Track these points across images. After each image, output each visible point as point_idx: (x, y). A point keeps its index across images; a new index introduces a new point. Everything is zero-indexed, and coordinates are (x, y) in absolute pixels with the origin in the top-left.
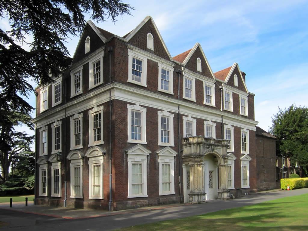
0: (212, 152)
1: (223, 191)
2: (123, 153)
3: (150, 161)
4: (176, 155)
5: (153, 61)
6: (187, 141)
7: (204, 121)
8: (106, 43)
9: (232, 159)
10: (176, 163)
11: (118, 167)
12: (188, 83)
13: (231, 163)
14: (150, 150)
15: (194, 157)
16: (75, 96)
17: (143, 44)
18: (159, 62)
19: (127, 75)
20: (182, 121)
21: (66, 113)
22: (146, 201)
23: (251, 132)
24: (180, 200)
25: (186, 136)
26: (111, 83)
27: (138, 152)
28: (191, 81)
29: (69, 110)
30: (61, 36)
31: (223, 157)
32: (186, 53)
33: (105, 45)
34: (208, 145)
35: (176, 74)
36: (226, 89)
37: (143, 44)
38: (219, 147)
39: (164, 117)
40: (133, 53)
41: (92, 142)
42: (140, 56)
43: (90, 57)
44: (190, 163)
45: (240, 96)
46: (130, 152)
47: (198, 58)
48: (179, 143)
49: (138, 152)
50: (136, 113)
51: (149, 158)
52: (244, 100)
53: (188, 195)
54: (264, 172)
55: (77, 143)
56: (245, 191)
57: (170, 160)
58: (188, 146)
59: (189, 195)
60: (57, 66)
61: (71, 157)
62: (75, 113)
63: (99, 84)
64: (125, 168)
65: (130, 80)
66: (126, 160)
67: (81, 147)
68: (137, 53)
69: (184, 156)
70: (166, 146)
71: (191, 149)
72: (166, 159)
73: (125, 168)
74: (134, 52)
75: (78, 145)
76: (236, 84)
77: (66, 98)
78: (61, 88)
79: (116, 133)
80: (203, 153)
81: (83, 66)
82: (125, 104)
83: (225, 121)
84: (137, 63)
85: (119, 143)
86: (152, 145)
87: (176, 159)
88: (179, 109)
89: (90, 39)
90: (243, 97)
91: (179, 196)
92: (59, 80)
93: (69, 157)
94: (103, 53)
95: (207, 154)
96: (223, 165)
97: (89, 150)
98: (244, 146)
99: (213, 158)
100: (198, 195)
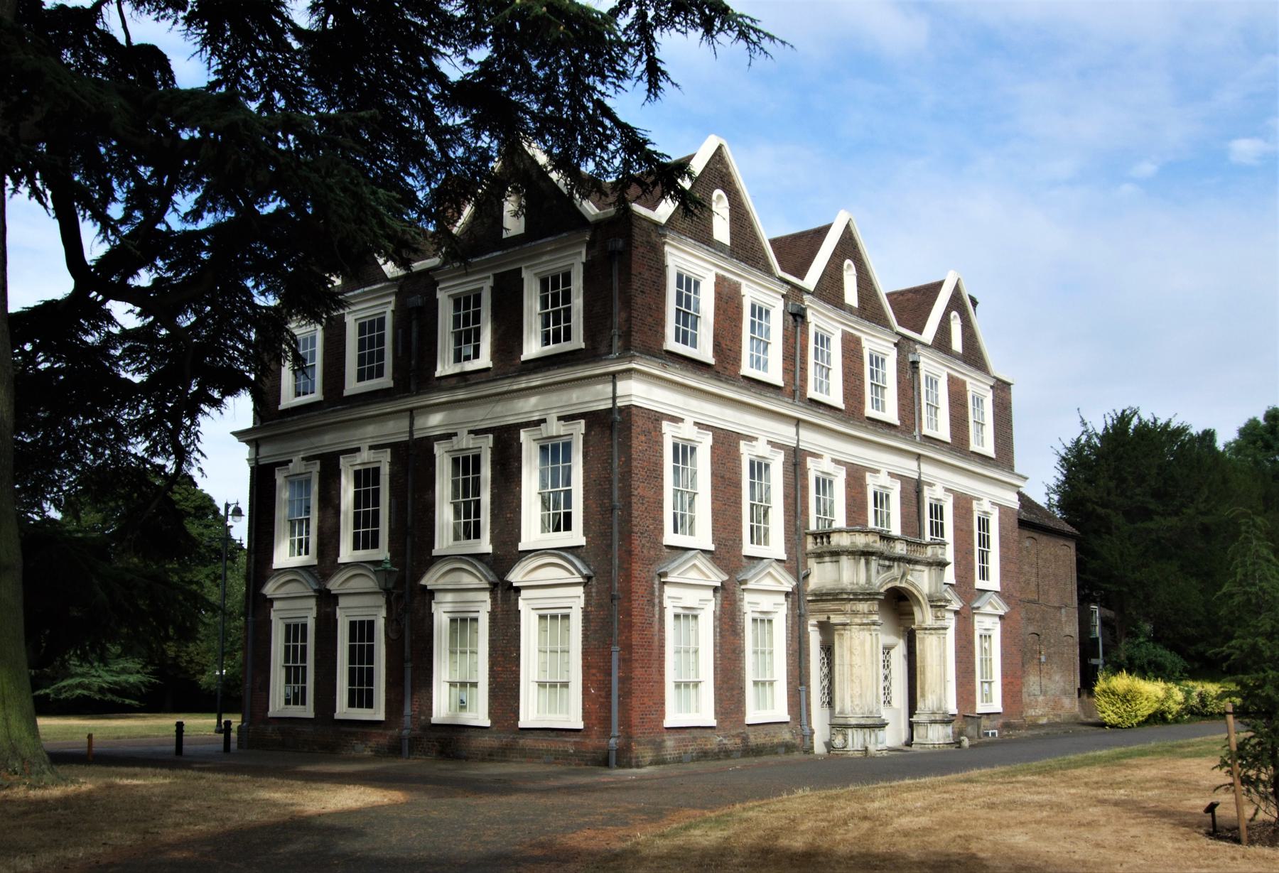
2: (653, 578)
12: (688, 289)
14: (728, 573)
18: (743, 282)
21: (412, 424)
23: (1004, 510)
27: (692, 576)
38: (918, 567)
39: (756, 460)
41: (532, 533)
45: (969, 387)
47: (848, 262)
63: (564, 347)
70: (762, 559)
71: (839, 571)
72: (766, 599)
73: (656, 627)
79: (635, 513)
81: (495, 275)
82: (656, 418)
84: (688, 284)
88: (797, 434)
90: (978, 388)
93: (430, 580)
99: (898, 604)
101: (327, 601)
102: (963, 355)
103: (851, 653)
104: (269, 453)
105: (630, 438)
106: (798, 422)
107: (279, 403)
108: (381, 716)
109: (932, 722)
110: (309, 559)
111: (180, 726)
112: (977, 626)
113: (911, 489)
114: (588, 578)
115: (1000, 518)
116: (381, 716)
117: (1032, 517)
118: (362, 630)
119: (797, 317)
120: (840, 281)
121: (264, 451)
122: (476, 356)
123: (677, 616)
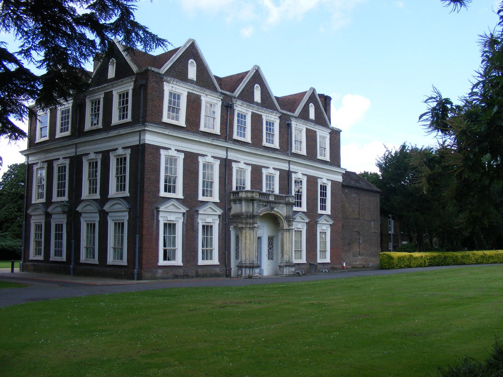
0: (271, 211)
1: (285, 264)
2: (154, 209)
3: (187, 220)
4: (221, 214)
5: (195, 94)
6: (237, 196)
7: (263, 169)
8: (138, 74)
9: (304, 221)
10: (221, 224)
11: (148, 226)
13: (300, 225)
14: (187, 206)
15: (245, 217)
16: (91, 129)
17: (183, 74)
19: (162, 113)
20: (231, 169)
21: (76, 150)
22: (181, 272)
23: (334, 183)
24: (226, 272)
25: (237, 189)
26: (142, 125)
27: (172, 209)
28: (245, 116)
29: (81, 147)
30: (81, 59)
31: (286, 219)
32: (241, 76)
33: (136, 76)
34: (266, 202)
35: (225, 108)
36: (297, 125)
37: (183, 74)
38: (280, 205)
40: (170, 86)
41: (113, 191)
42: (178, 89)
43: (115, 85)
44: (240, 226)
45: (318, 134)
46: (162, 208)
48: (227, 198)
49: (172, 209)
50: (171, 159)
51: (186, 216)
52: (324, 138)
53: (237, 266)
54: (359, 242)
55: (92, 191)
56: (322, 266)
57: (213, 220)
58: (237, 202)
59: (238, 267)
60: (69, 89)
61: (82, 209)
62: (91, 151)
64: (155, 227)
65: (165, 119)
66: (157, 218)
67: (97, 196)
68: (174, 86)
69: (233, 216)
72: (210, 217)
73: (155, 227)
74: (171, 85)
75: (93, 194)
76: (312, 116)
77: (78, 130)
78: (70, 114)
79: (146, 184)
80: (257, 213)
81: (105, 93)
82: (157, 149)
83: (293, 168)
84: (175, 97)
85: (149, 197)
86: (191, 203)
87: (221, 219)
88: (227, 153)
89: (116, 63)
90: (323, 134)
91: (224, 268)
92: (68, 105)
93: (79, 209)
94: (132, 84)
95: (263, 213)
96: (286, 230)
97: (109, 202)
98: (323, 203)
99: (274, 220)
100: (250, 267)
101: (48, 216)
103: (246, 239)
104: (32, 159)
106: (227, 149)
107: (35, 140)
108: (51, 259)
109: (286, 266)
110: (43, 200)
112: (318, 229)
114: (130, 209)
116: (51, 259)
118: (59, 227)
119: (286, 128)
121: (30, 159)
122: (98, 124)
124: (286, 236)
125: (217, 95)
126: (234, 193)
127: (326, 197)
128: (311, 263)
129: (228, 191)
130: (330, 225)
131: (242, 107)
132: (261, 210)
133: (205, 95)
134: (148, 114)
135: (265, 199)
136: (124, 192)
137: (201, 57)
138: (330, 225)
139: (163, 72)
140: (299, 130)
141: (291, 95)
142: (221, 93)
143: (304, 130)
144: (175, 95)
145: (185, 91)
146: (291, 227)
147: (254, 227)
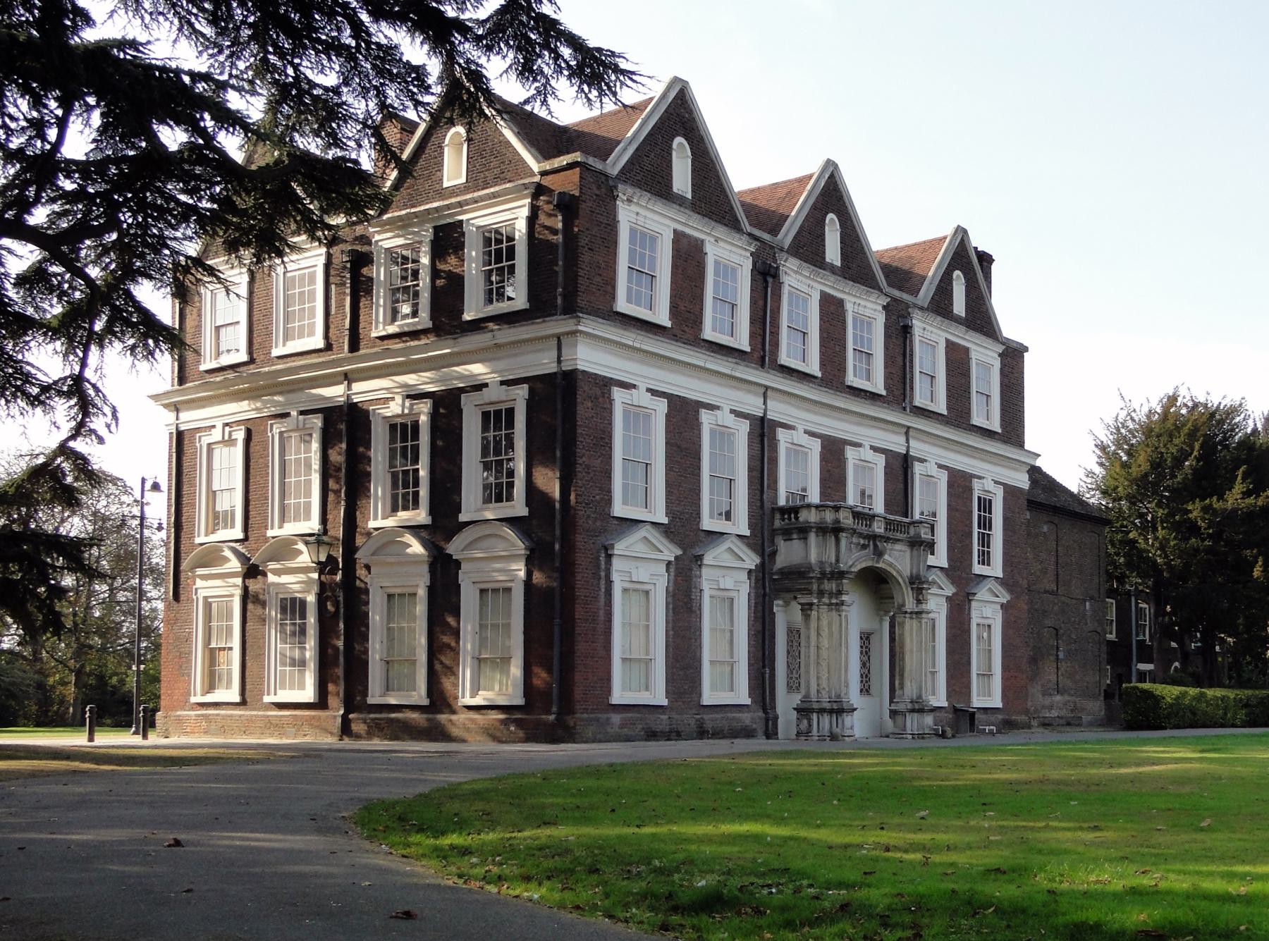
14: (680, 544)
19: (614, 287)
32: (786, 190)
41: (472, 504)
45: (973, 355)
46: (620, 548)
47: (831, 216)
58: (795, 536)
59: (798, 710)
72: (727, 576)
73: (602, 600)
81: (435, 228)
82: (605, 384)
85: (589, 517)
88: (765, 403)
90: (984, 356)
91: (761, 714)
99: (876, 583)
100: (831, 712)
102: (966, 319)
105: (575, 405)
106: (766, 391)
109: (913, 711)
111: (91, 739)
112: (974, 614)
113: (897, 465)
115: (1004, 499)
117: (1042, 497)
120: (821, 237)
123: (625, 590)
124: (911, 629)
125: (741, 241)
126: (784, 511)
127: (990, 529)
128: (958, 706)
129: (767, 505)
130: (1002, 605)
131: (798, 277)
132: (854, 559)
133: (712, 240)
134: (582, 288)
135: (862, 529)
136: (509, 504)
137: (702, 132)
138: (1002, 605)
139: (615, 171)
140: (931, 338)
141: (896, 248)
142: (750, 235)
143: (943, 345)
144: (643, 235)
145: (669, 227)
146: (924, 606)
147: (842, 603)
